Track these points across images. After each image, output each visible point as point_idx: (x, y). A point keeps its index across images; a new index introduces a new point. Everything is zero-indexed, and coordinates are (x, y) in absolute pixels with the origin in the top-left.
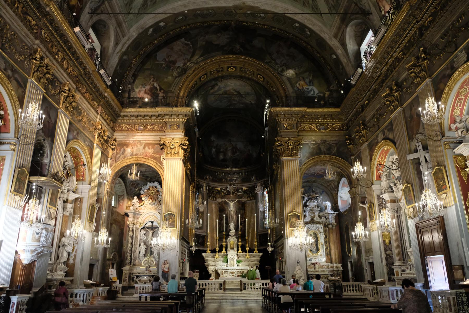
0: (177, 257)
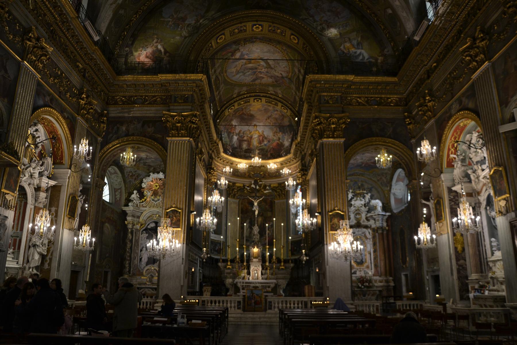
0: (183, 266)
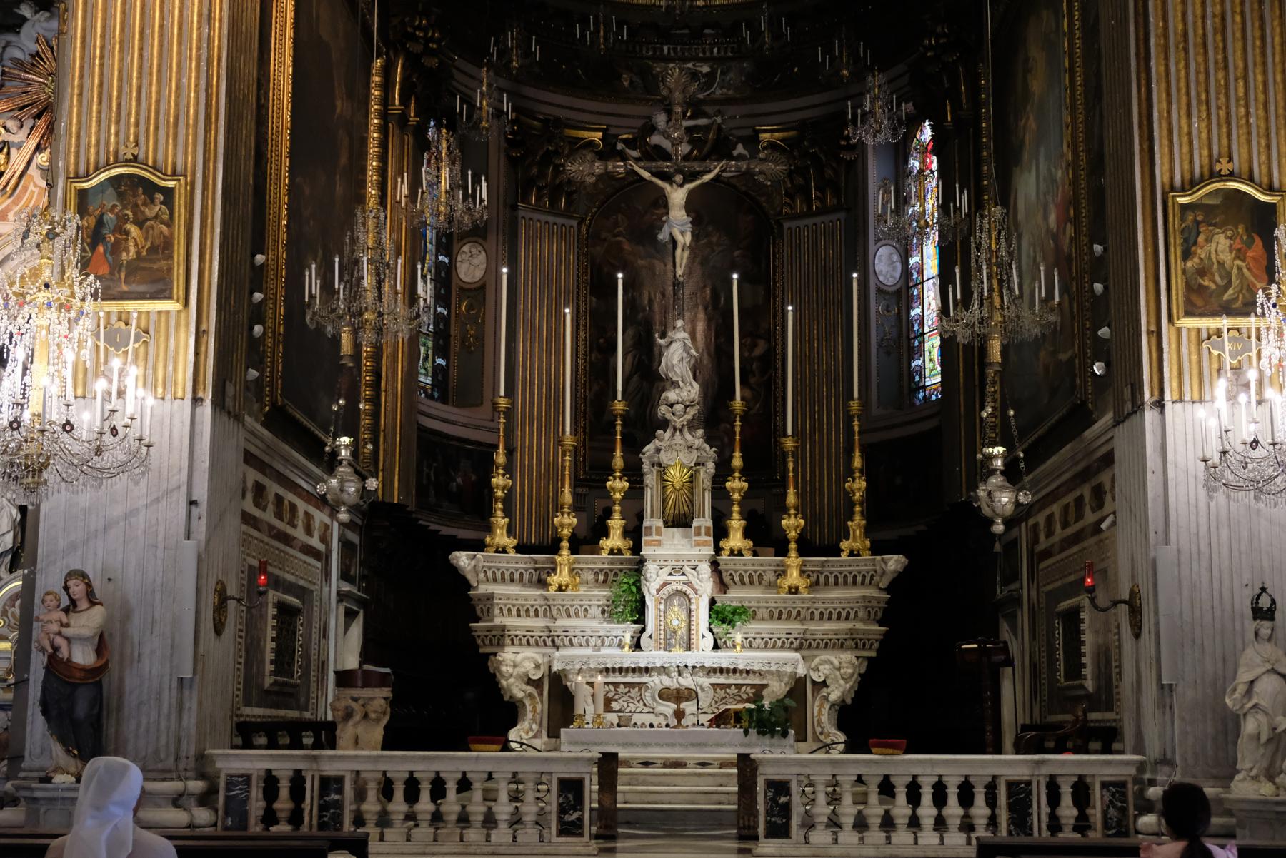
0: (189, 551)
